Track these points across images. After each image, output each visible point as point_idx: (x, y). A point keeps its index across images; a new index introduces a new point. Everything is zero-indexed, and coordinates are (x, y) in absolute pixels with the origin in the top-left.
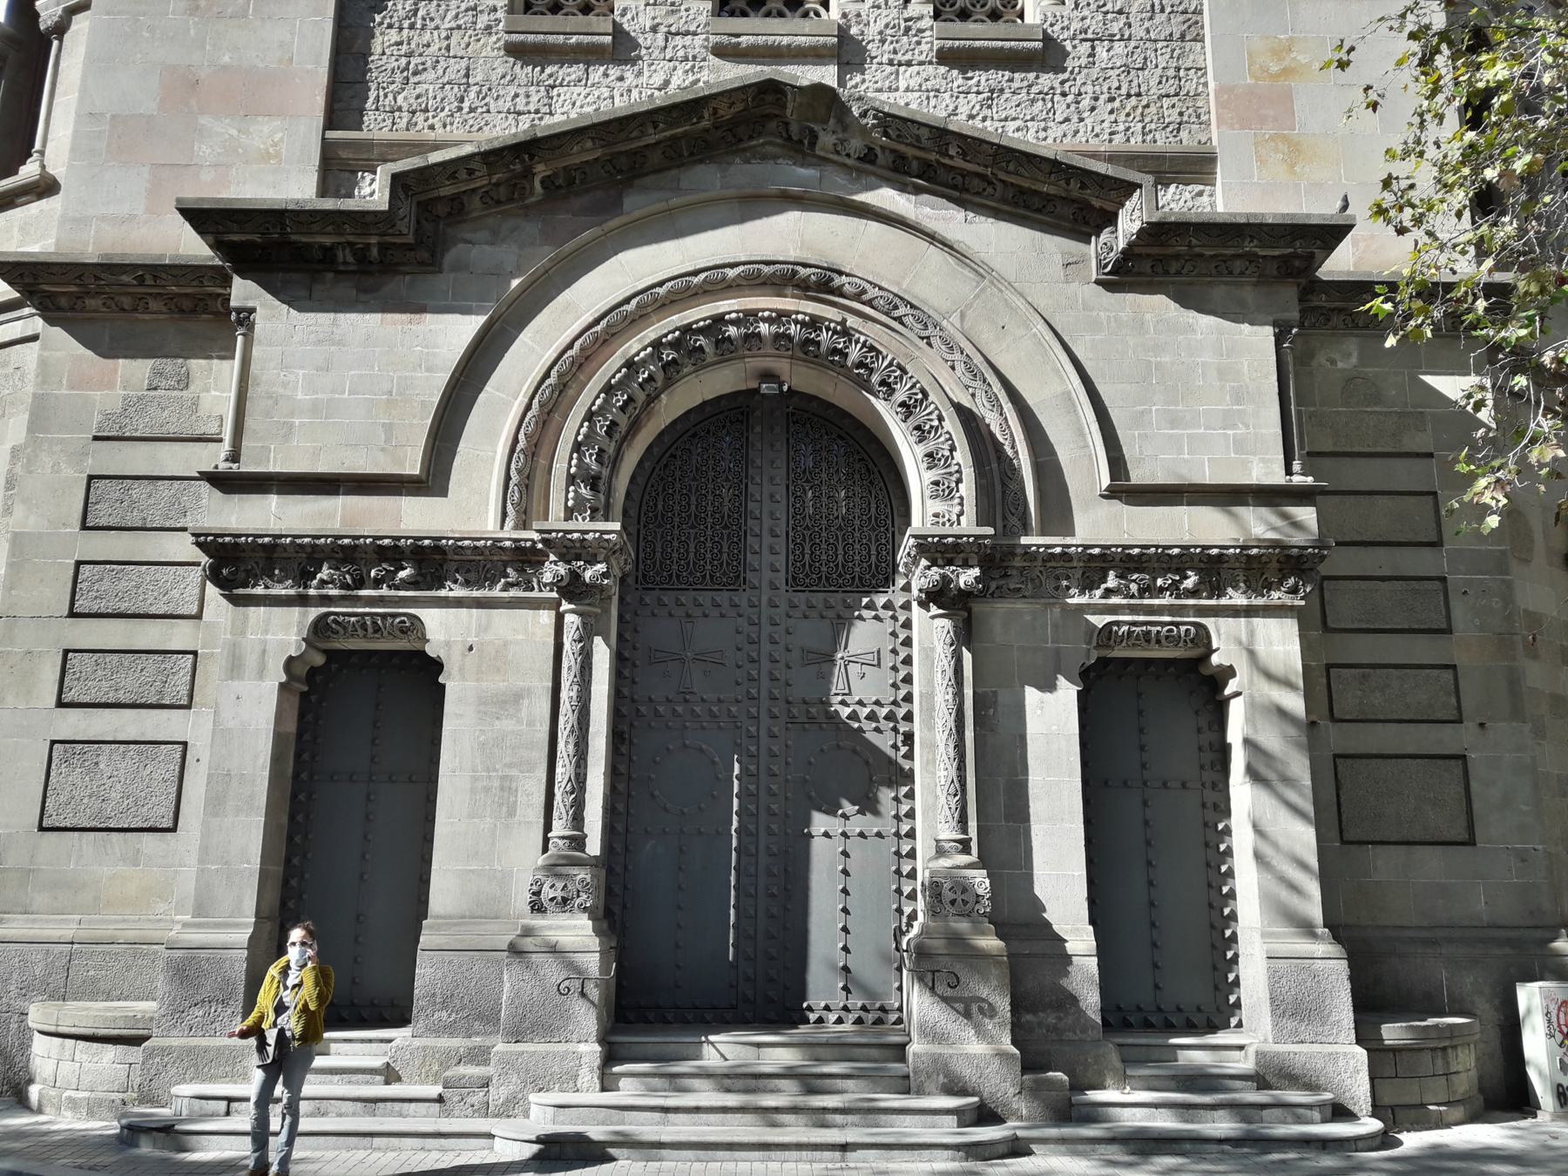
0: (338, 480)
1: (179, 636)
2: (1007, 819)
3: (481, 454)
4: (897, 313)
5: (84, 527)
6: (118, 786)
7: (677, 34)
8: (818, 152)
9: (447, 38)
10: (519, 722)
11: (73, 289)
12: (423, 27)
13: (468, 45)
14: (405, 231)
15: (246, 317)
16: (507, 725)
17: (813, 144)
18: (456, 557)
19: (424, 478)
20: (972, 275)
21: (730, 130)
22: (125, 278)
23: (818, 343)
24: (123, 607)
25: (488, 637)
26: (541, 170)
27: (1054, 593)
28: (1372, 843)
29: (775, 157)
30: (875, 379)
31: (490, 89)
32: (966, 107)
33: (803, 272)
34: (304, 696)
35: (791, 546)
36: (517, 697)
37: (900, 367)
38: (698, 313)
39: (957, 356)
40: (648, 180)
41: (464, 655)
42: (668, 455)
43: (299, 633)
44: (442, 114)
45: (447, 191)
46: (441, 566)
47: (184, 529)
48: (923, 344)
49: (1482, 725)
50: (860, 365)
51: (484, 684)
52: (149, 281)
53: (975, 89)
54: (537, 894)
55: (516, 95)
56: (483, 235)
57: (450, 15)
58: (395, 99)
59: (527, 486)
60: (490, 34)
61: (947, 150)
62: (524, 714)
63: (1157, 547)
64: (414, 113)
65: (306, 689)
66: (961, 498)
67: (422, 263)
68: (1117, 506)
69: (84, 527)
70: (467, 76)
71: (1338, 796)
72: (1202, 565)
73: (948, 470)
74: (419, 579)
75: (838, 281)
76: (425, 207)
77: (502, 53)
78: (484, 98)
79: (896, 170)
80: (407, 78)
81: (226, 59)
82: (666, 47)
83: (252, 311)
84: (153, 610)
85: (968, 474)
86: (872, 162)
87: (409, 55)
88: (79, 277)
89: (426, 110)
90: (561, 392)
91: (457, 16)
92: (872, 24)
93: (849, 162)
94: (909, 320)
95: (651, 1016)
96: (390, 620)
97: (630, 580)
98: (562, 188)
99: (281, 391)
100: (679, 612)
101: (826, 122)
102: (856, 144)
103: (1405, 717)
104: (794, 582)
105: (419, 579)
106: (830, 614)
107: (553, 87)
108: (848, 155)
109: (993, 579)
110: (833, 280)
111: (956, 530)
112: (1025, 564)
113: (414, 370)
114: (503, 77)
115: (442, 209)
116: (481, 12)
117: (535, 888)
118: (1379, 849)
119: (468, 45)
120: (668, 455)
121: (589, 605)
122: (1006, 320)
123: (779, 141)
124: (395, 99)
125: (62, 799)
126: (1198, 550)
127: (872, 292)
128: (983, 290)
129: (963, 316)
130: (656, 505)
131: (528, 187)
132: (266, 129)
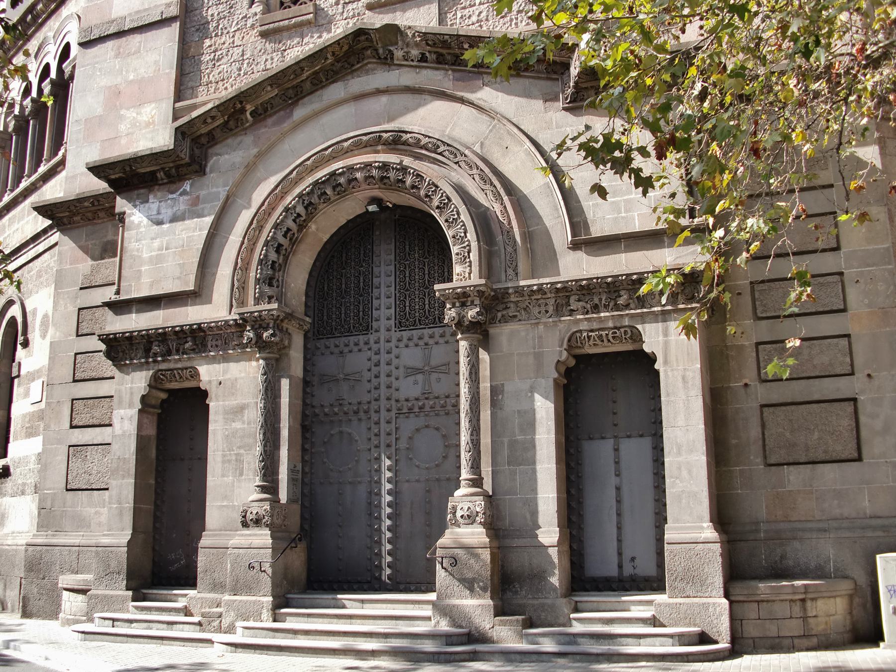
1: (104, 388)
2: (509, 464)
4: (439, 150)
5: (78, 336)
6: (95, 467)
8: (396, 62)
9: (233, 36)
10: (243, 423)
11: (67, 214)
12: (222, 33)
13: (243, 37)
14: (183, 156)
15: (122, 217)
16: (237, 425)
17: (392, 58)
18: (210, 333)
20: (487, 118)
21: (346, 61)
22: (86, 204)
23: (389, 177)
24: (94, 374)
25: (228, 376)
26: (249, 108)
28: (788, 464)
29: (373, 70)
30: (422, 193)
33: (385, 135)
35: (398, 303)
36: (242, 409)
37: (433, 184)
39: (475, 171)
40: (306, 99)
41: (217, 387)
42: (330, 256)
43: (145, 383)
45: (204, 130)
47: (94, 334)
48: (456, 167)
49: (869, 376)
52: (96, 203)
54: (244, 517)
55: (266, 60)
58: (209, 77)
60: (254, 29)
61: (462, 46)
62: (245, 418)
64: (217, 83)
65: (160, 411)
66: (470, 262)
67: (196, 172)
69: (78, 336)
70: (243, 55)
71: (763, 434)
72: (630, 287)
74: (195, 347)
75: (405, 137)
76: (196, 140)
80: (214, 64)
81: (131, 77)
82: (343, 12)
83: (124, 213)
84: (106, 375)
85: (474, 245)
86: (426, 61)
87: (215, 52)
88: (69, 208)
89: (223, 80)
90: (260, 231)
91: (237, 24)
93: (415, 63)
95: (335, 587)
96: (185, 371)
97: (310, 335)
98: (262, 114)
99: (136, 253)
101: (397, 44)
102: (415, 52)
103: (813, 375)
104: (400, 325)
105: (195, 347)
106: (421, 343)
107: (285, 50)
108: (412, 60)
109: (498, 311)
110: (402, 137)
112: (518, 299)
113: (194, 232)
114: (260, 51)
115: (204, 140)
116: (249, 17)
117: (243, 514)
118: (792, 468)
119: (243, 37)
120: (330, 256)
121: (269, 353)
122: (508, 143)
123: (375, 60)
124: (209, 77)
125: (74, 475)
127: (424, 141)
129: (482, 144)
130: (324, 287)
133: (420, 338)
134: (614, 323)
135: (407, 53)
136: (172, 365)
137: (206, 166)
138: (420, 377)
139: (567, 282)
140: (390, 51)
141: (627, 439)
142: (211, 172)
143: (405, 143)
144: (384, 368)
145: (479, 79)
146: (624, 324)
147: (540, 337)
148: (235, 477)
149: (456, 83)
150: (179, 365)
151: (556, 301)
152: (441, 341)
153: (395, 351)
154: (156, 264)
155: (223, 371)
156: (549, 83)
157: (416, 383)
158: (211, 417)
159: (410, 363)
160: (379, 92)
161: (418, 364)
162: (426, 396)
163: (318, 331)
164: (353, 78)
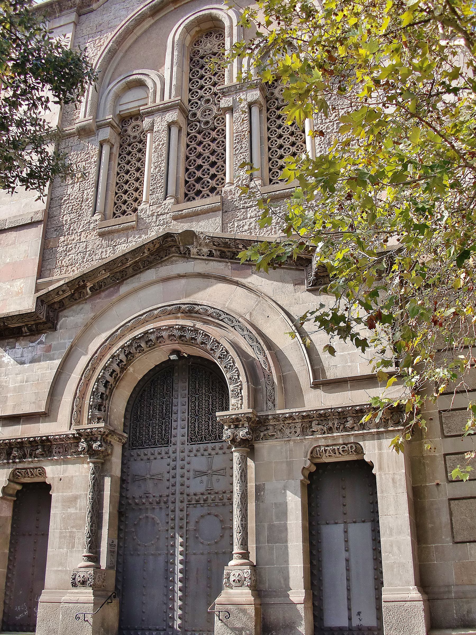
0: (20, 416)
3: (66, 400)
4: (221, 318)
7: (161, 215)
9: (80, 235)
16: (72, 510)
17: (189, 254)
19: (47, 412)
25: (66, 475)
26: (89, 285)
27: (289, 435)
31: (93, 252)
32: (275, 220)
33: (183, 307)
34: (309, 486)
35: (190, 424)
36: (75, 498)
38: (138, 332)
42: (142, 390)
44: (77, 265)
46: (51, 447)
48: (232, 329)
50: (202, 343)
51: (65, 494)
53: (278, 211)
55: (102, 252)
56: (70, 313)
57: (81, 227)
59: (80, 411)
62: (78, 505)
63: (331, 409)
64: (67, 266)
65: (15, 499)
67: (50, 328)
68: (319, 392)
70: (86, 248)
73: (237, 385)
76: (51, 306)
77: (98, 237)
78: (91, 256)
79: (221, 257)
81: (8, 261)
86: (213, 256)
92: (236, 194)
93: (205, 257)
94: (226, 320)
97: (126, 446)
99: (5, 384)
100: (145, 458)
101: (193, 244)
102: (205, 250)
104: (191, 440)
106: (206, 453)
107: (115, 246)
108: (203, 255)
109: (262, 431)
111: (240, 411)
113: (46, 370)
115: (56, 306)
120: (142, 390)
126: (350, 408)
127: (210, 311)
128: (259, 302)
129: (251, 313)
130: (137, 412)
131: (85, 292)
132: (18, 283)
133: (205, 450)
134: (343, 440)
135: (200, 250)
136: (26, 466)
137: (57, 324)
138: (205, 478)
139: (310, 411)
140: (188, 248)
141: (353, 524)
142: (60, 328)
143: (197, 312)
144: (179, 471)
145: (249, 269)
146: (350, 441)
147: (291, 450)
148: (68, 548)
149: (232, 270)
150: (31, 466)
151: (302, 425)
152: (221, 452)
153: (187, 459)
154: (18, 392)
155: (63, 471)
156: (298, 272)
157: (202, 482)
158: (53, 504)
159: (198, 468)
160: (180, 276)
161: (204, 469)
162: (209, 492)
163: (132, 443)
164: (162, 266)
